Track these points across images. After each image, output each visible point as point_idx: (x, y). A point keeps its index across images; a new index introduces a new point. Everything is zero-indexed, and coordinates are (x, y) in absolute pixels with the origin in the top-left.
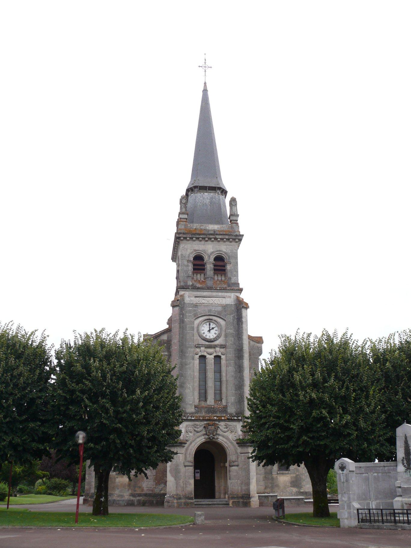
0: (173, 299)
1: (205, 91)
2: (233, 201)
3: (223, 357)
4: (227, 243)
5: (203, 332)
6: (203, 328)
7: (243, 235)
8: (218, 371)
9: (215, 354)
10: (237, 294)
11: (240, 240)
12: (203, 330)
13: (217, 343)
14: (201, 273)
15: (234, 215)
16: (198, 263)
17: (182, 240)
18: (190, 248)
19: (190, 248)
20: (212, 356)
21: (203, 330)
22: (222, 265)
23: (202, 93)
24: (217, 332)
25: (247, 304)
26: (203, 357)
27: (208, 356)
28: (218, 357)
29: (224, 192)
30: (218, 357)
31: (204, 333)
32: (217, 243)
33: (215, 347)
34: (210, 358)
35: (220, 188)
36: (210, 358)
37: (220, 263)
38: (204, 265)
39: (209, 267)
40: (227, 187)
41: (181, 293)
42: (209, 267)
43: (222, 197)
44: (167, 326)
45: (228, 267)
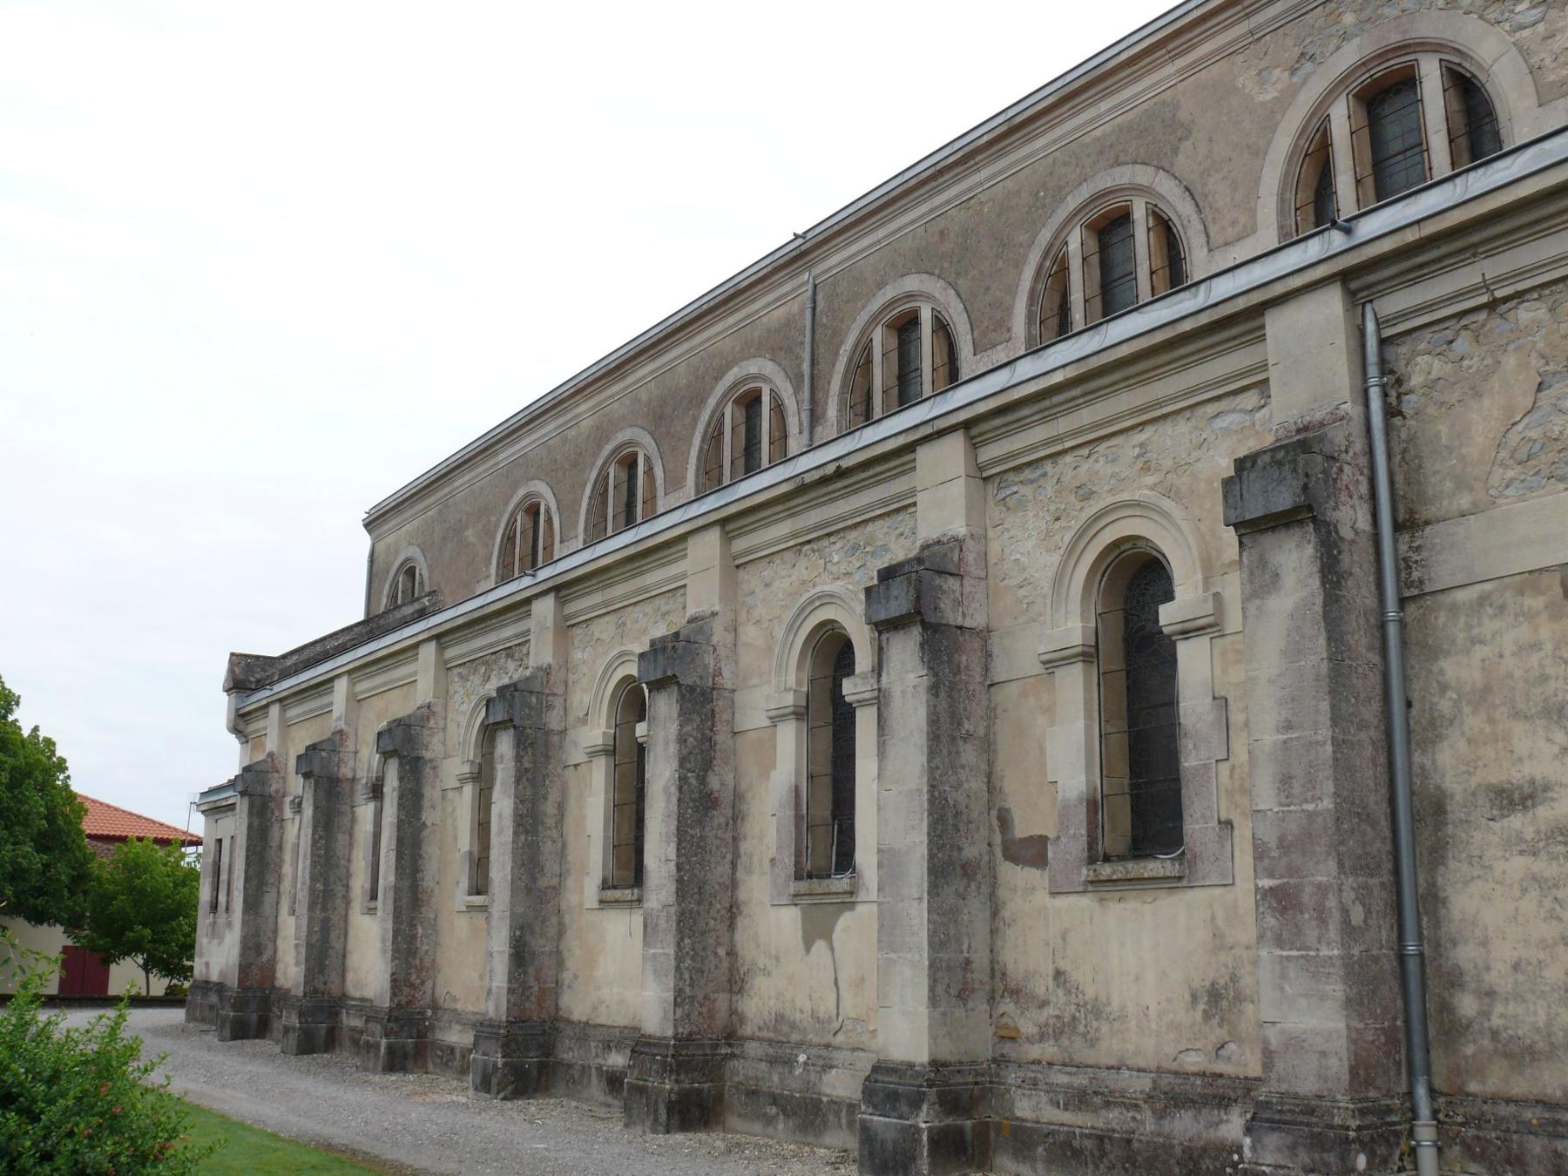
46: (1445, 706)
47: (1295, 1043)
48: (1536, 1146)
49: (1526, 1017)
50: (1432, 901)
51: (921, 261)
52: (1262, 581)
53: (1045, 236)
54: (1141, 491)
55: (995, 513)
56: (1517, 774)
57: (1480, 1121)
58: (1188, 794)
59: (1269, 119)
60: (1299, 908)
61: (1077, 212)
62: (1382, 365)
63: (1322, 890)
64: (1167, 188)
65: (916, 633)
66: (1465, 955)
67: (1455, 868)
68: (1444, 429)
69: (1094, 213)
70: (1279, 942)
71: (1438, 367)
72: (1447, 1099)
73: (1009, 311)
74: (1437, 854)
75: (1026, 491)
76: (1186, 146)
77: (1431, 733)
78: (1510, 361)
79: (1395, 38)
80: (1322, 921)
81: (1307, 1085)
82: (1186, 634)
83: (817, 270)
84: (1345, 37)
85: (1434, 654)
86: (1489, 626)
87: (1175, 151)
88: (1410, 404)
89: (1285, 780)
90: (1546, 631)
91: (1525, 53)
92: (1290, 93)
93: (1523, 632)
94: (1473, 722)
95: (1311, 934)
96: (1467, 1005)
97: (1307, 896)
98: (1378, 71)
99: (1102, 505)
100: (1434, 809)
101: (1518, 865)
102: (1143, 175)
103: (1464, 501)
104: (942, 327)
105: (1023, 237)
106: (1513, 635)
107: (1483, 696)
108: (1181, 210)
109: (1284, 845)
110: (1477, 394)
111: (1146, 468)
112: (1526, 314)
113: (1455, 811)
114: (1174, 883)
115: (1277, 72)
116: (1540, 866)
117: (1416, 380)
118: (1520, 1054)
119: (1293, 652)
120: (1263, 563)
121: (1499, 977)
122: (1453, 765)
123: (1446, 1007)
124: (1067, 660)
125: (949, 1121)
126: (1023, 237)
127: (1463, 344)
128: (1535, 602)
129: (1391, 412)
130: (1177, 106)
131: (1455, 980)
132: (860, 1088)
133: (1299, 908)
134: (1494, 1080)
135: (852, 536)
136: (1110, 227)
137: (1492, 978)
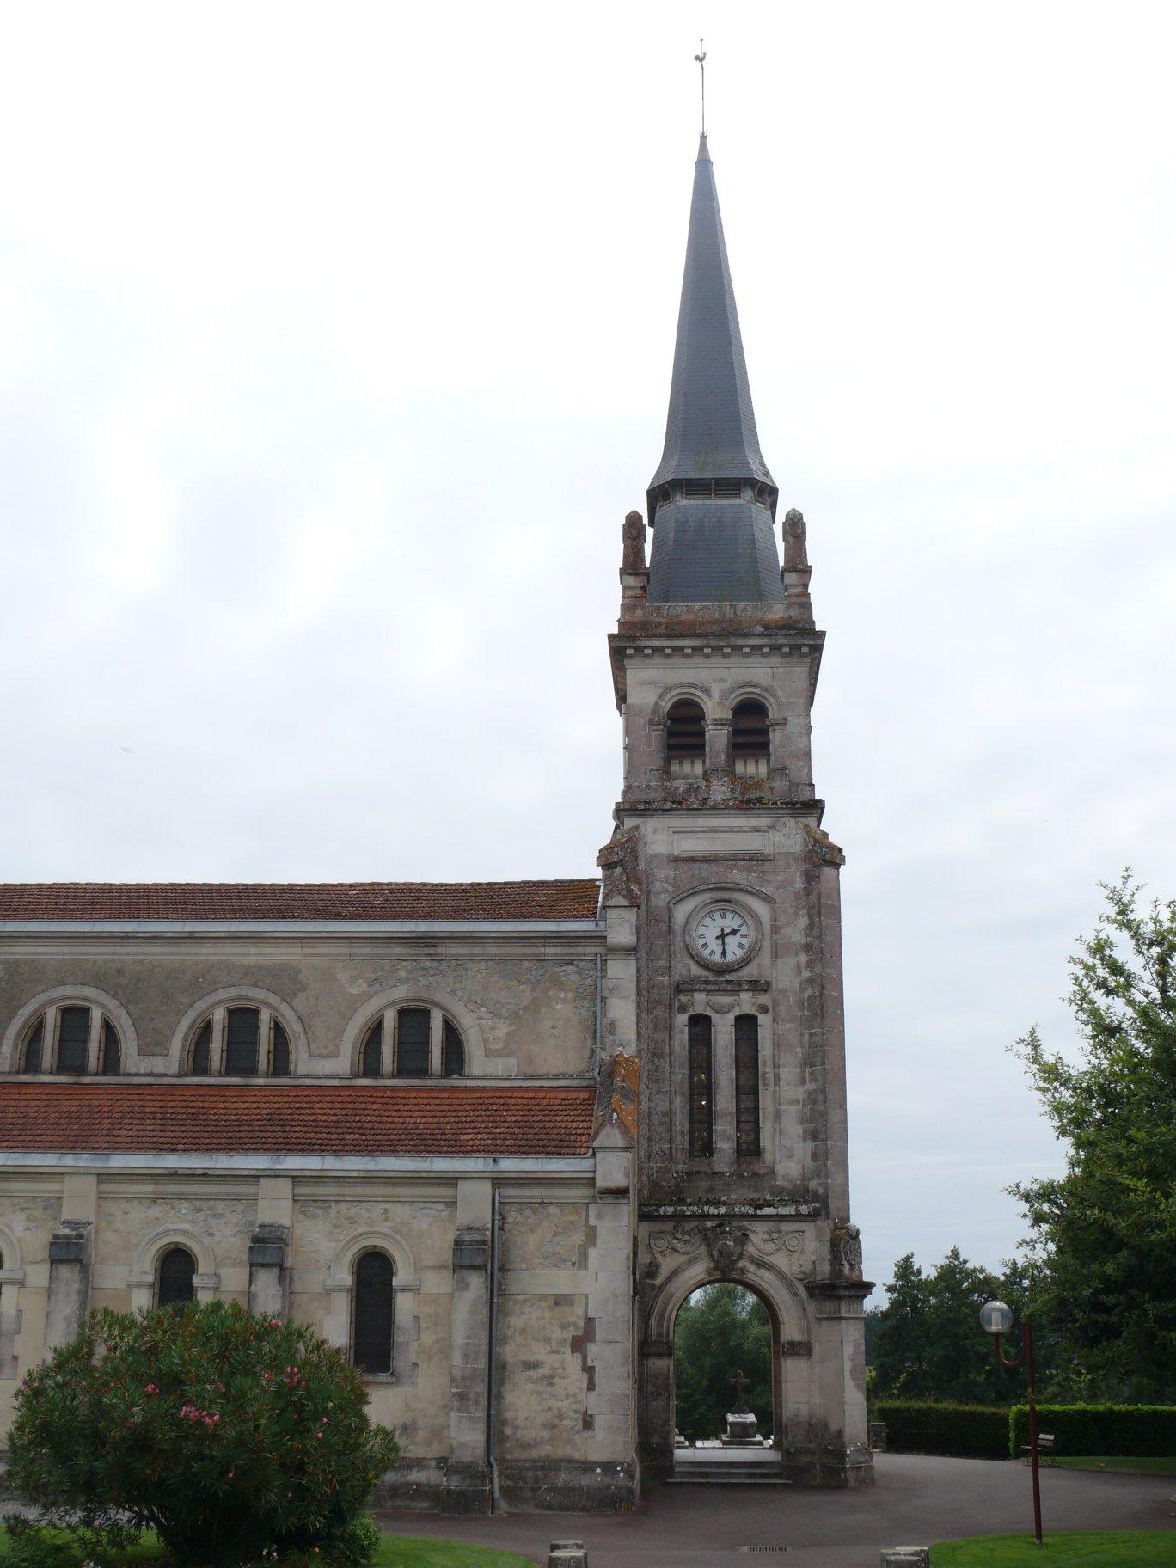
0: (606, 841)
1: (704, 165)
2: (796, 528)
4: (713, 660)
5: (702, 941)
6: (702, 930)
7: (824, 633)
8: (747, 1058)
10: (812, 821)
11: (817, 649)
13: (745, 974)
14: (693, 758)
15: (799, 567)
17: (630, 657)
18: (657, 681)
19: (657, 681)
20: (731, 1017)
22: (753, 727)
23: (693, 171)
24: (744, 941)
26: (701, 1023)
27: (715, 1017)
28: (746, 1025)
29: (767, 493)
30: (746, 1025)
31: (705, 945)
32: (683, 660)
34: (724, 1033)
36: (724, 1033)
37: (749, 723)
39: (717, 738)
41: (630, 823)
42: (717, 738)
43: (759, 509)
44: (592, 871)
45: (776, 736)
47: (463, 1445)
48: (530, 1474)
49: (527, 1434)
50: (499, 1397)
51: (97, 979)
52: (463, 1286)
53: (201, 1005)
54: (384, 1228)
56: (532, 1358)
57: (512, 1468)
58: (395, 1353)
59: (355, 1003)
60: (468, 1399)
61: (225, 1001)
62: (499, 1210)
63: (478, 1394)
64: (285, 1010)
66: (509, 1415)
67: (508, 1386)
68: (519, 1239)
69: (234, 1004)
70: (459, 1410)
71: (519, 1218)
72: (501, 1460)
73: (169, 1039)
74: (502, 1382)
75: (319, 1212)
76: (302, 995)
77: (504, 1341)
79: (425, 996)
81: (467, 1458)
82: (403, 1290)
84: (401, 981)
85: (506, 1315)
86: (527, 1309)
87: (295, 995)
88: (507, 1227)
90: (547, 1314)
92: (366, 998)
94: (519, 1339)
95: (472, 1409)
96: (508, 1431)
97: (472, 1395)
98: (413, 1004)
101: (530, 1386)
102: (273, 1000)
103: (524, 1266)
104: (108, 1028)
105: (184, 999)
107: (523, 1331)
108: (293, 1027)
109: (464, 1378)
110: (532, 1231)
111: (387, 1219)
112: (552, 1209)
113: (509, 1368)
114: (388, 1385)
115: (360, 981)
116: (537, 1387)
117: (510, 1220)
118: (526, 1446)
119: (473, 1313)
120: (463, 1280)
121: (520, 1421)
122: (510, 1352)
124: (340, 1290)
125: (1002, 1411)
128: (543, 1304)
129: (501, 1229)
130: (299, 972)
131: (505, 1423)
132: (633, 1446)
133: (468, 1399)
135: (198, 1203)
137: (518, 1422)
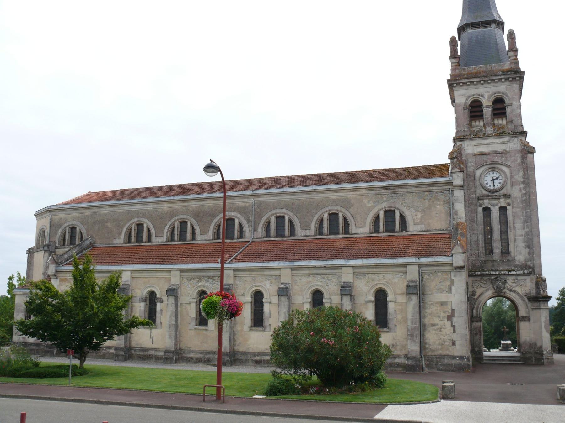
2: (511, 35)
3: (508, 207)
5: (486, 182)
6: (486, 178)
9: (500, 205)
10: (523, 139)
12: (486, 180)
13: (502, 192)
14: (479, 120)
15: (514, 49)
16: (474, 110)
17: (455, 87)
18: (465, 94)
19: (465, 94)
21: (486, 180)
22: (500, 107)
24: (501, 181)
25: (451, 38)
26: (487, 210)
27: (492, 208)
28: (503, 210)
29: (500, 24)
30: (503, 210)
31: (487, 183)
33: (499, 197)
34: (495, 213)
35: (495, 21)
36: (495, 213)
37: (499, 106)
38: (504, 109)
39: (487, 112)
40: (504, 19)
41: (458, 143)
42: (487, 112)
46: (426, 314)
47: (412, 350)
48: (435, 360)
50: (424, 335)
55: (356, 279)
56: (434, 323)
58: (389, 322)
59: (370, 209)
62: (421, 275)
65: (349, 296)
66: (427, 341)
69: (330, 212)
73: (310, 224)
74: (424, 330)
75: (362, 277)
77: (425, 317)
78: (437, 279)
79: (392, 205)
80: (416, 337)
83: (255, 199)
85: (425, 309)
86: (432, 307)
89: (412, 322)
91: (412, 216)
92: (374, 207)
93: (436, 308)
94: (430, 317)
96: (427, 346)
98: (389, 209)
99: (376, 283)
100: (425, 325)
101: (434, 332)
102: (343, 210)
106: (435, 308)
107: (431, 314)
109: (412, 329)
112: (439, 274)
113: (427, 326)
119: (414, 308)
122: (427, 321)
123: (425, 346)
126: (314, 211)
127: (431, 275)
131: (426, 343)
132: (469, 351)
134: (430, 353)
136: (333, 216)
